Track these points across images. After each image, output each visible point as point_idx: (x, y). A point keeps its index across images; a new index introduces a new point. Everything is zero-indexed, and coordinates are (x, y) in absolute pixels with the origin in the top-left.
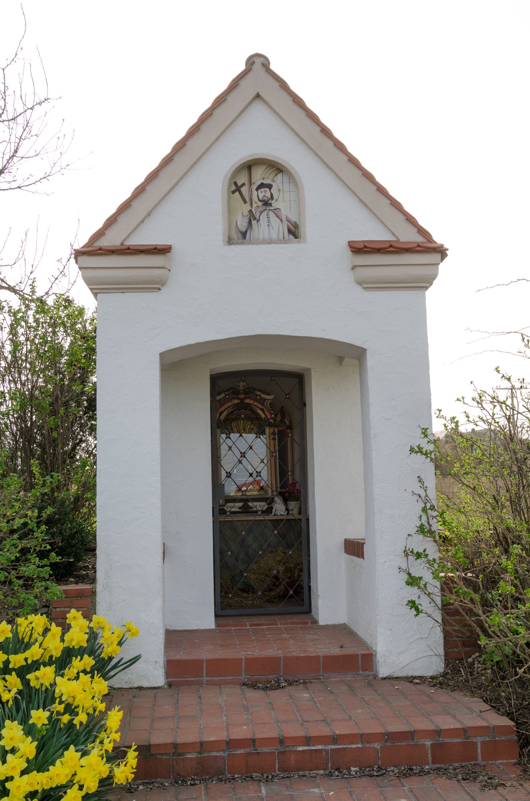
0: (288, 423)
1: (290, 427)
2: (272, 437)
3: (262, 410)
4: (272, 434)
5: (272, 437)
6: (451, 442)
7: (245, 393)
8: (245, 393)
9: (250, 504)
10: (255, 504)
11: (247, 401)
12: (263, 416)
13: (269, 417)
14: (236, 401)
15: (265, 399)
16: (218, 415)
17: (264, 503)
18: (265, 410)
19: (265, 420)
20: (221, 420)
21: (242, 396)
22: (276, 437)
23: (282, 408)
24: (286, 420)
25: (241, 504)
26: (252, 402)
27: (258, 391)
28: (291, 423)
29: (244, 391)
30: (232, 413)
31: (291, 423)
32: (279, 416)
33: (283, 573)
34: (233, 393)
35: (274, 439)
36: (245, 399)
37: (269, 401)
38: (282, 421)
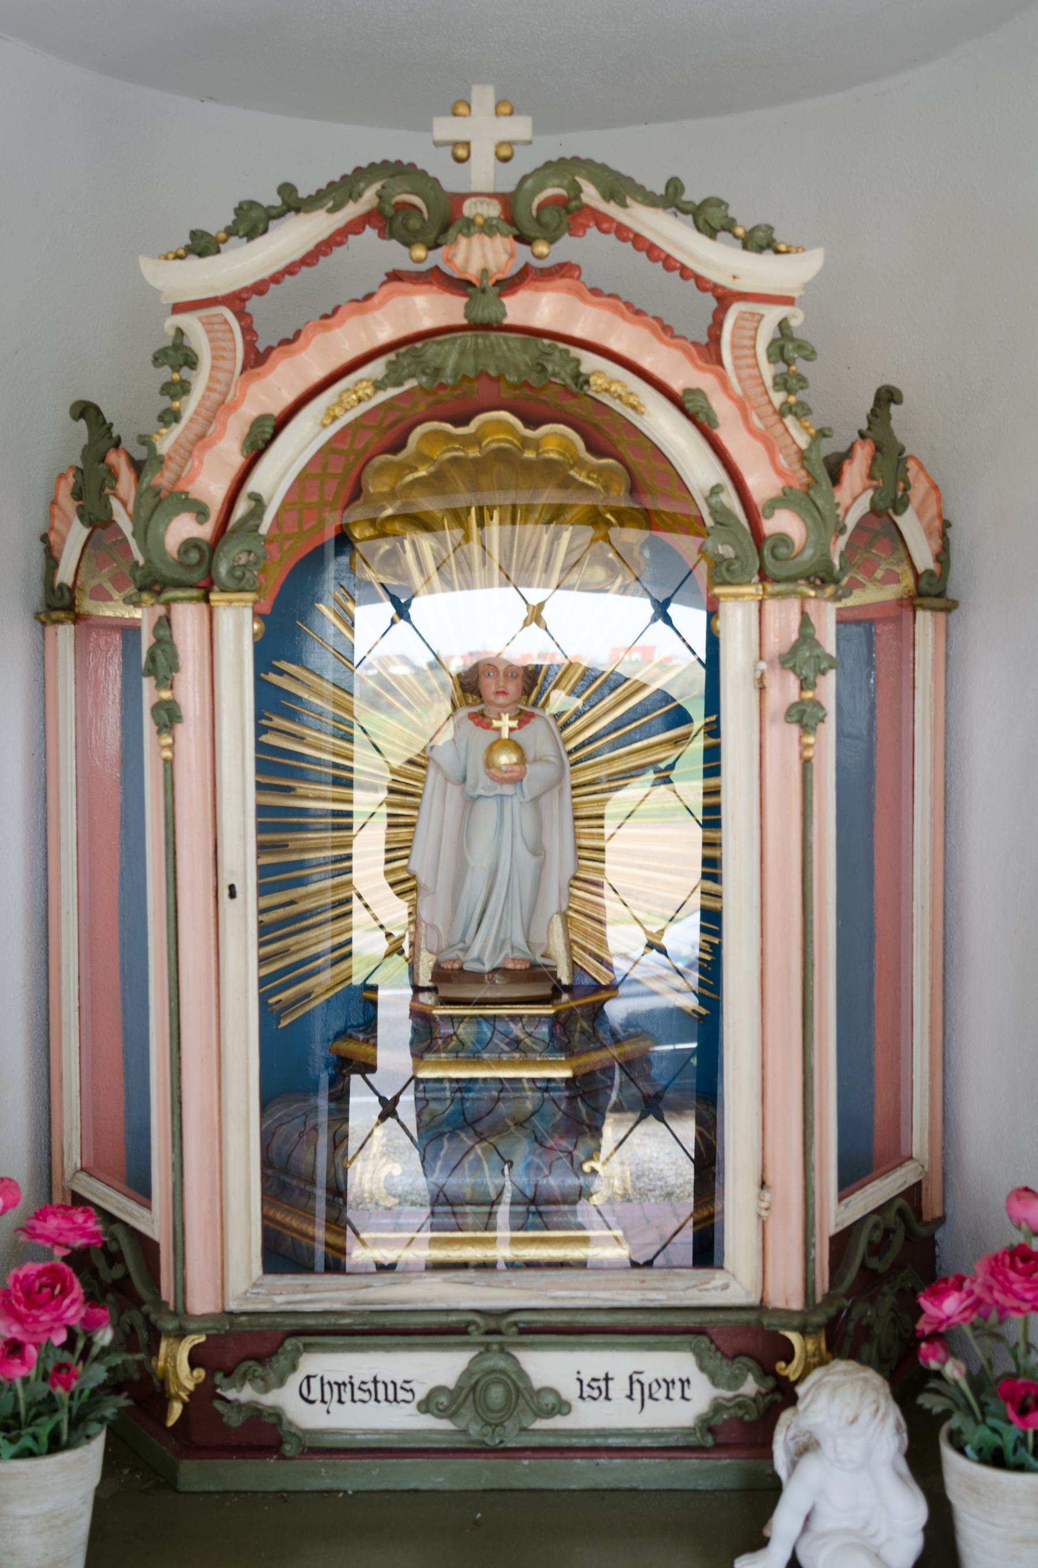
0: (924, 558)
1: (933, 592)
2: (785, 690)
3: (688, 406)
4: (788, 660)
5: (785, 690)
6: (368, 677)
7: (518, 221)
8: (518, 221)
9: (548, 1367)
10: (594, 1362)
11: (540, 308)
12: (699, 470)
13: (762, 483)
14: (428, 309)
15: (725, 298)
16: (229, 451)
17: (677, 1363)
18: (721, 407)
19: (721, 514)
20: (259, 502)
21: (482, 255)
22: (828, 688)
23: (887, 397)
24: (908, 523)
25: (443, 1367)
26: (586, 321)
27: (651, 200)
28: (943, 556)
29: (507, 201)
30: (389, 432)
31: (943, 556)
32: (855, 473)
33: (610, 1201)
34: (386, 220)
35: (803, 716)
36: (509, 285)
37: (773, 314)
38: (881, 526)
